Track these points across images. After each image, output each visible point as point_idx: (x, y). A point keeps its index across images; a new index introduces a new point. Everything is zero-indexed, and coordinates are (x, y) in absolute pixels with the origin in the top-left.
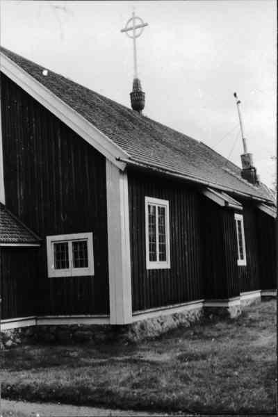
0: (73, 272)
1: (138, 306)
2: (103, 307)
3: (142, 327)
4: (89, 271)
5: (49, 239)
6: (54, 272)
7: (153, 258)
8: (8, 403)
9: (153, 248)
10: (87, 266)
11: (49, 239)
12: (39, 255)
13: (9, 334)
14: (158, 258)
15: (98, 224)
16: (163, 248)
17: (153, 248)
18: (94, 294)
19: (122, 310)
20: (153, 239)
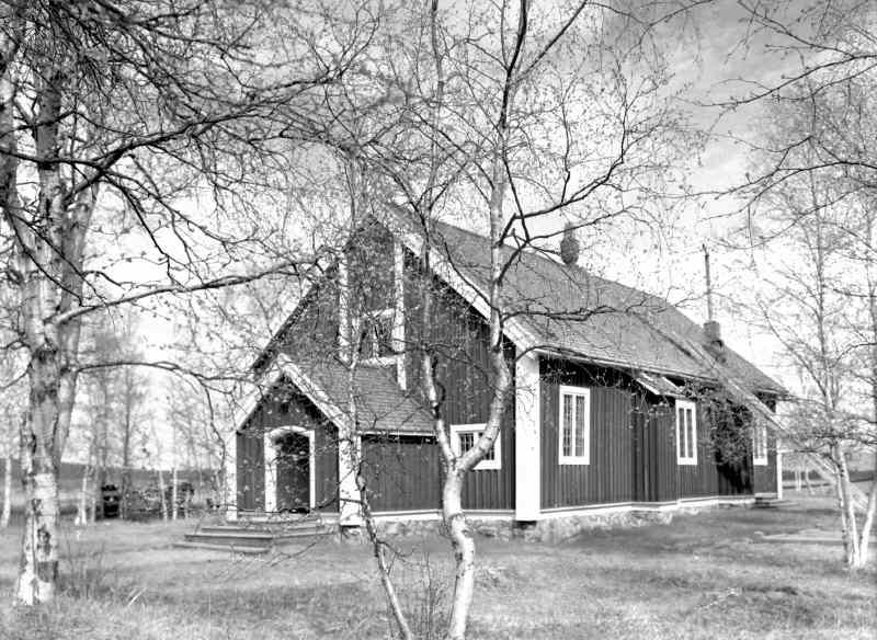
1: (547, 502)
3: (552, 526)
4: (496, 464)
9: (567, 441)
17: (567, 441)
19: (528, 502)
20: (567, 431)
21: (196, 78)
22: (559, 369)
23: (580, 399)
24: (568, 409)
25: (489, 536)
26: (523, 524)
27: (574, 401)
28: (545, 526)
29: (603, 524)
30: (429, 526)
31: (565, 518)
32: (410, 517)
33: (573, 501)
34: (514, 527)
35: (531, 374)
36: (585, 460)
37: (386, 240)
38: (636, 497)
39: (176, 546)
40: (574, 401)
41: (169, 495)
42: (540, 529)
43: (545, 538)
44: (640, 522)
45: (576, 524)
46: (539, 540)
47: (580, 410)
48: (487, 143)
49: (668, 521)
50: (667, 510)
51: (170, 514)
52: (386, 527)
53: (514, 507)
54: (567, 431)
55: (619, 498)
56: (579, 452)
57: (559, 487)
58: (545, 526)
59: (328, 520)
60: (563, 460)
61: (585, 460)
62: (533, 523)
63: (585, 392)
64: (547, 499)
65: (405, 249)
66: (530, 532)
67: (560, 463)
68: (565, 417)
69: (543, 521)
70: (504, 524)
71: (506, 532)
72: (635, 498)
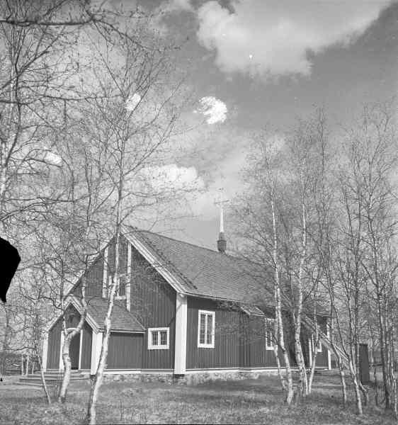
0: (159, 347)
1: (190, 365)
2: (171, 364)
3: (192, 377)
4: (167, 347)
5: (150, 329)
6: (151, 346)
7: (202, 342)
8: (371, 218)
9: (202, 336)
10: (153, 344)
11: (150, 329)
12: (143, 336)
13: (126, 376)
14: (206, 342)
15: (172, 323)
16: (203, 321)
17: (202, 336)
18: (167, 359)
19: (181, 366)
20: (202, 332)
21: (377, 191)
22: (196, 303)
23: (210, 317)
24: (203, 321)
25: (163, 382)
26: (177, 376)
27: (206, 317)
28: (189, 377)
29: (222, 378)
30: (137, 377)
31: (197, 373)
32: (227, 371)
33: (203, 365)
34: (173, 378)
35: (183, 305)
36: (212, 346)
37: (124, 244)
38: (241, 364)
39: (14, 384)
40: (206, 317)
41: (25, 363)
42: (186, 379)
43: (189, 383)
44: (242, 378)
45: (206, 377)
46: (185, 383)
47: (210, 322)
48: (41, 190)
49: (256, 378)
50: (255, 372)
51: (25, 371)
52: (113, 377)
53: (173, 368)
54: (202, 332)
55: (231, 365)
56: (209, 342)
57: (197, 358)
58: (189, 377)
59: (86, 374)
60: (200, 345)
61: (212, 346)
62: (183, 375)
63: (213, 313)
64: (191, 363)
65: (133, 247)
66: (181, 380)
67: (198, 346)
68: (201, 325)
69: (188, 375)
70: (169, 376)
71: (170, 380)
72: (240, 366)
